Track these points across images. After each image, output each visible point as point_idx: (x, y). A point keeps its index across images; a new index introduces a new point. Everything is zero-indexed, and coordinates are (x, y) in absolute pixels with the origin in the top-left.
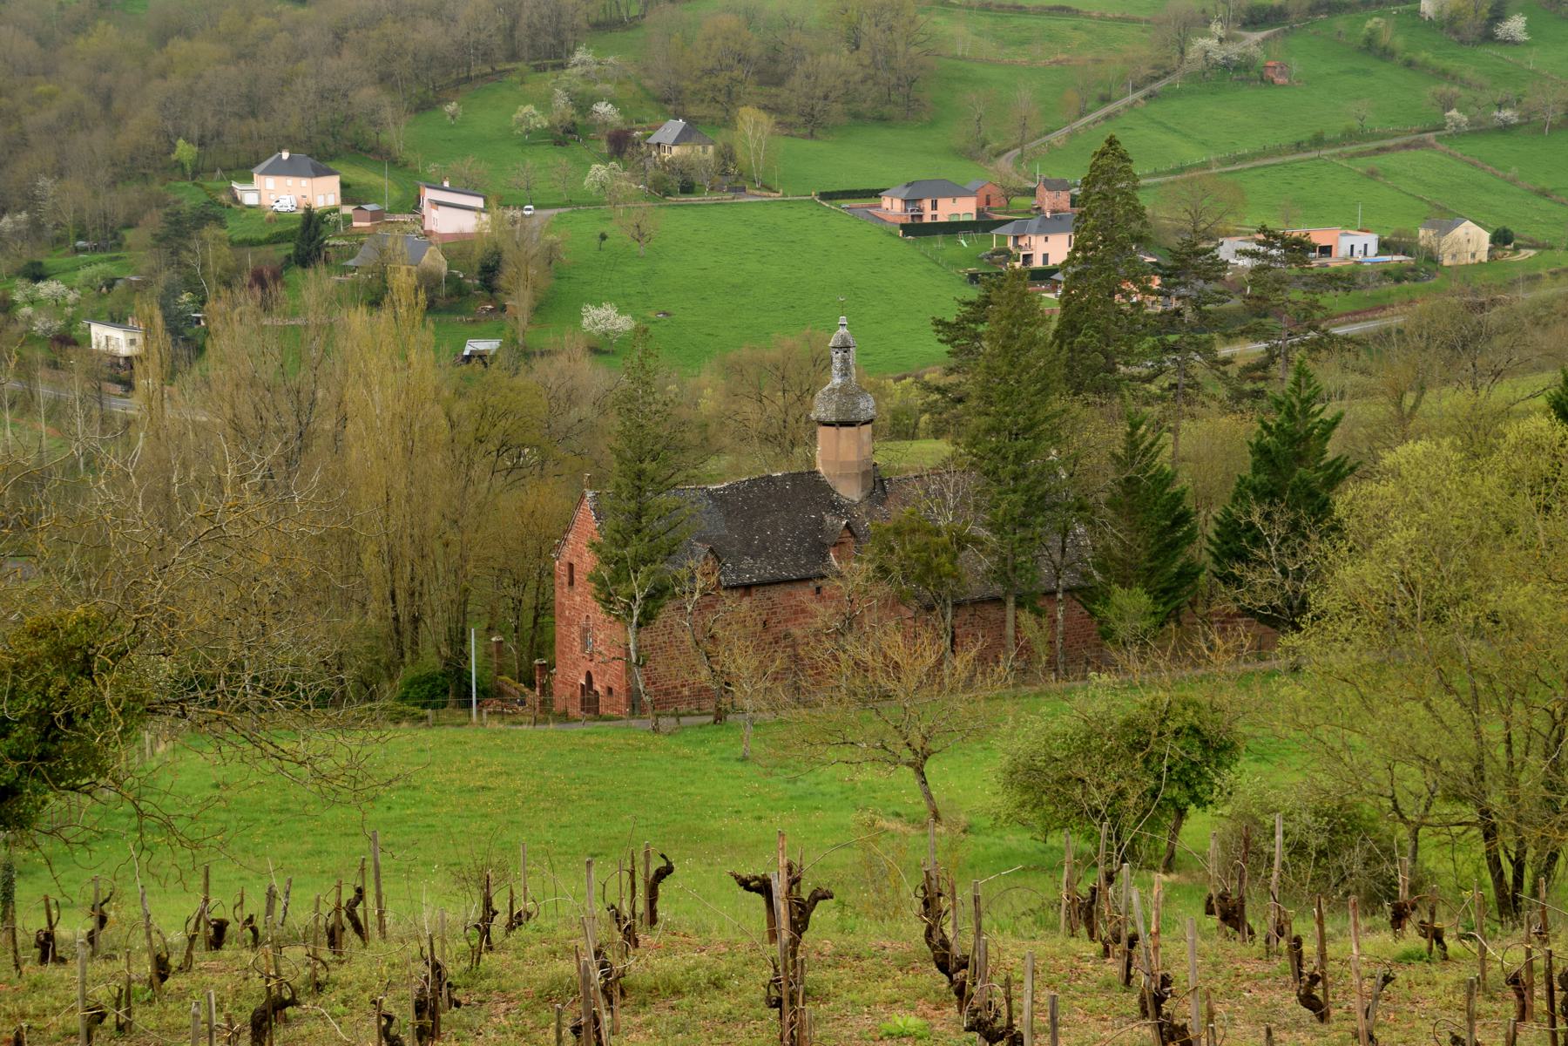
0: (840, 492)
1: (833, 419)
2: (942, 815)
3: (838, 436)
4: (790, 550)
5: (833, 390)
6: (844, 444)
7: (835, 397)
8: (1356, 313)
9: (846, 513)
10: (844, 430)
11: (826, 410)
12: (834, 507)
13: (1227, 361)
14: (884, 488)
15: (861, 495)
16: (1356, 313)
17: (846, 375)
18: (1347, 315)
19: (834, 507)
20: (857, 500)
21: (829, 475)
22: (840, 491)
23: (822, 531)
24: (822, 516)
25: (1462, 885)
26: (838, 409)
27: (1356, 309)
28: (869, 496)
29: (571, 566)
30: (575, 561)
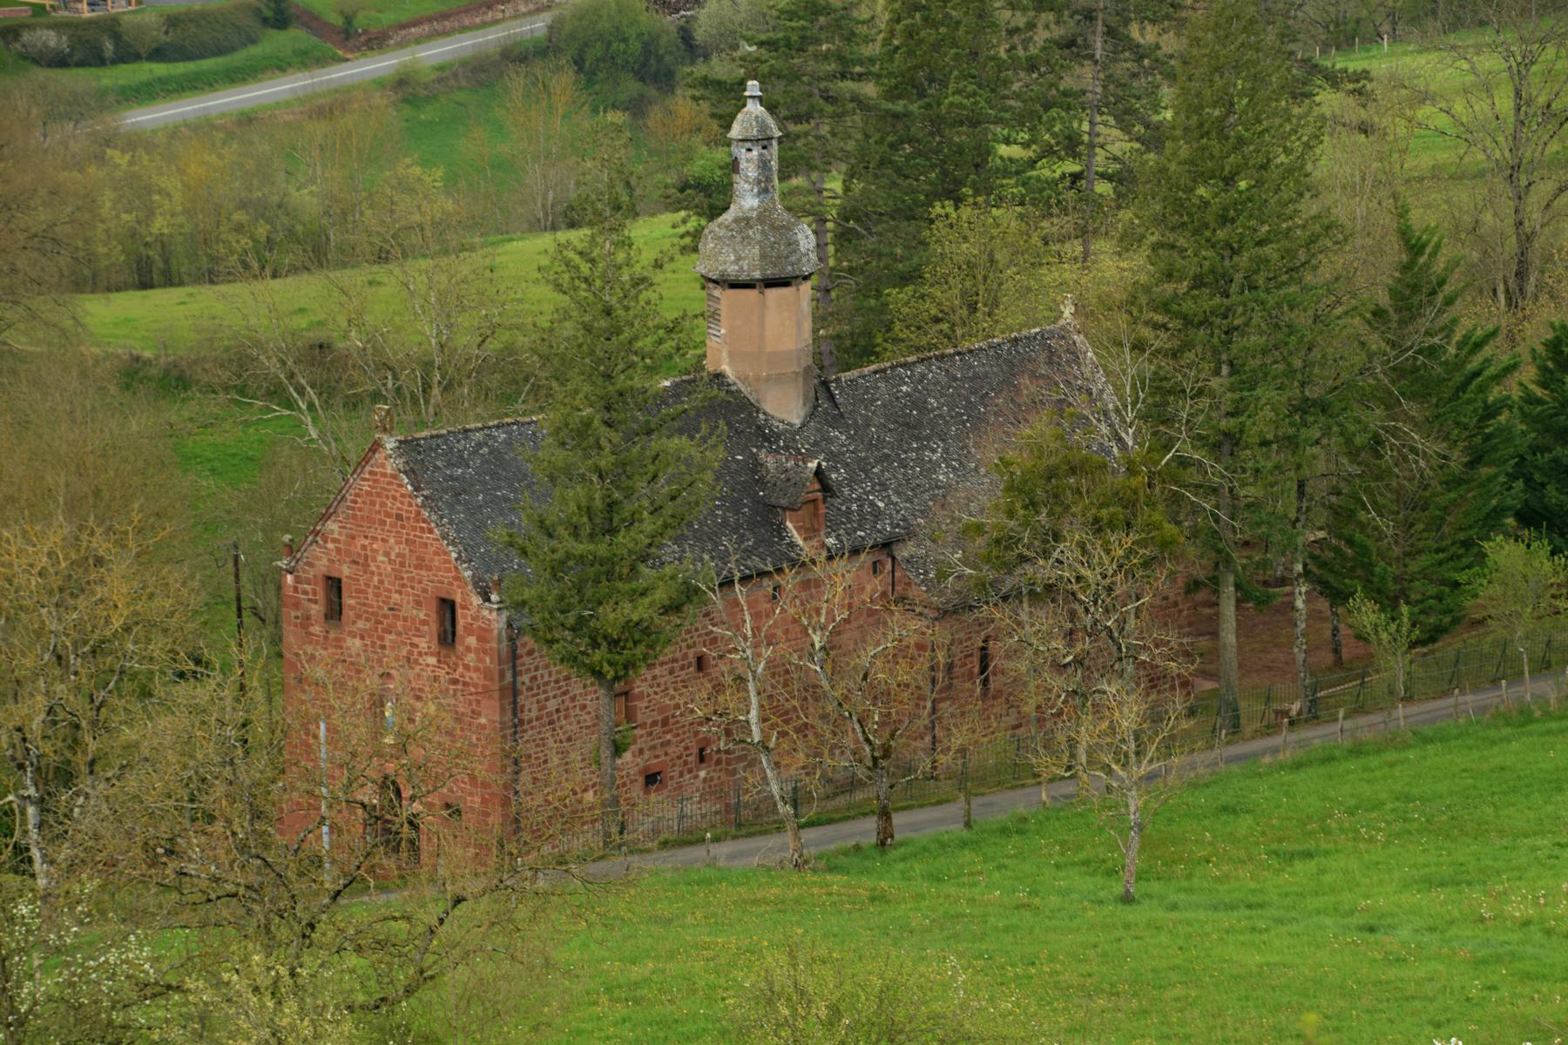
0: (768, 410)
1: (757, 275)
2: (426, 614)
3: (763, 305)
4: (725, 523)
5: (745, 221)
6: (773, 320)
7: (755, 233)
8: (444, 16)
9: (787, 448)
10: (773, 293)
11: (739, 259)
12: (766, 439)
13: (1098, 135)
14: (831, 397)
15: (802, 413)
16: (444, 16)
17: (766, 191)
18: (430, 19)
19: (766, 439)
20: (797, 422)
21: (745, 380)
22: (768, 407)
23: (761, 482)
24: (755, 457)
25: (35, 286)
26: (763, 256)
27: (443, 8)
28: (812, 415)
29: (334, 585)
30: (345, 571)
